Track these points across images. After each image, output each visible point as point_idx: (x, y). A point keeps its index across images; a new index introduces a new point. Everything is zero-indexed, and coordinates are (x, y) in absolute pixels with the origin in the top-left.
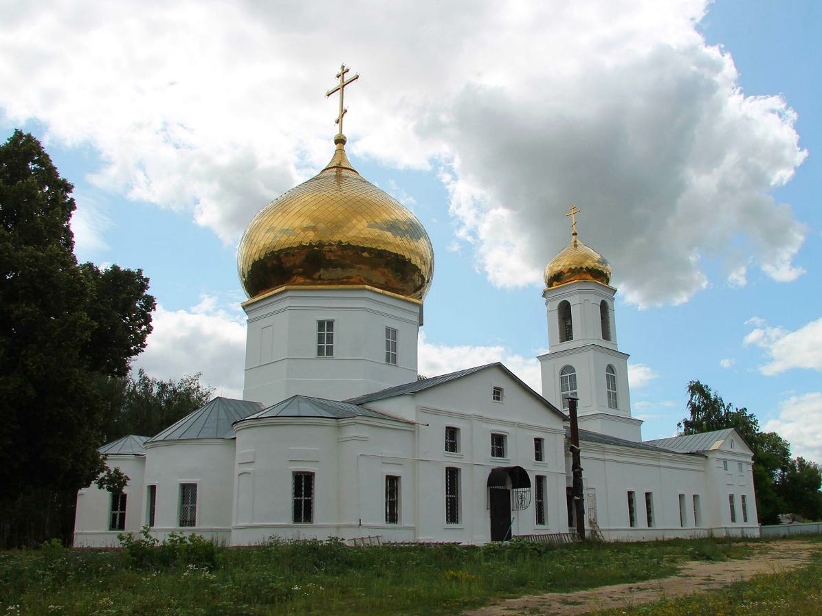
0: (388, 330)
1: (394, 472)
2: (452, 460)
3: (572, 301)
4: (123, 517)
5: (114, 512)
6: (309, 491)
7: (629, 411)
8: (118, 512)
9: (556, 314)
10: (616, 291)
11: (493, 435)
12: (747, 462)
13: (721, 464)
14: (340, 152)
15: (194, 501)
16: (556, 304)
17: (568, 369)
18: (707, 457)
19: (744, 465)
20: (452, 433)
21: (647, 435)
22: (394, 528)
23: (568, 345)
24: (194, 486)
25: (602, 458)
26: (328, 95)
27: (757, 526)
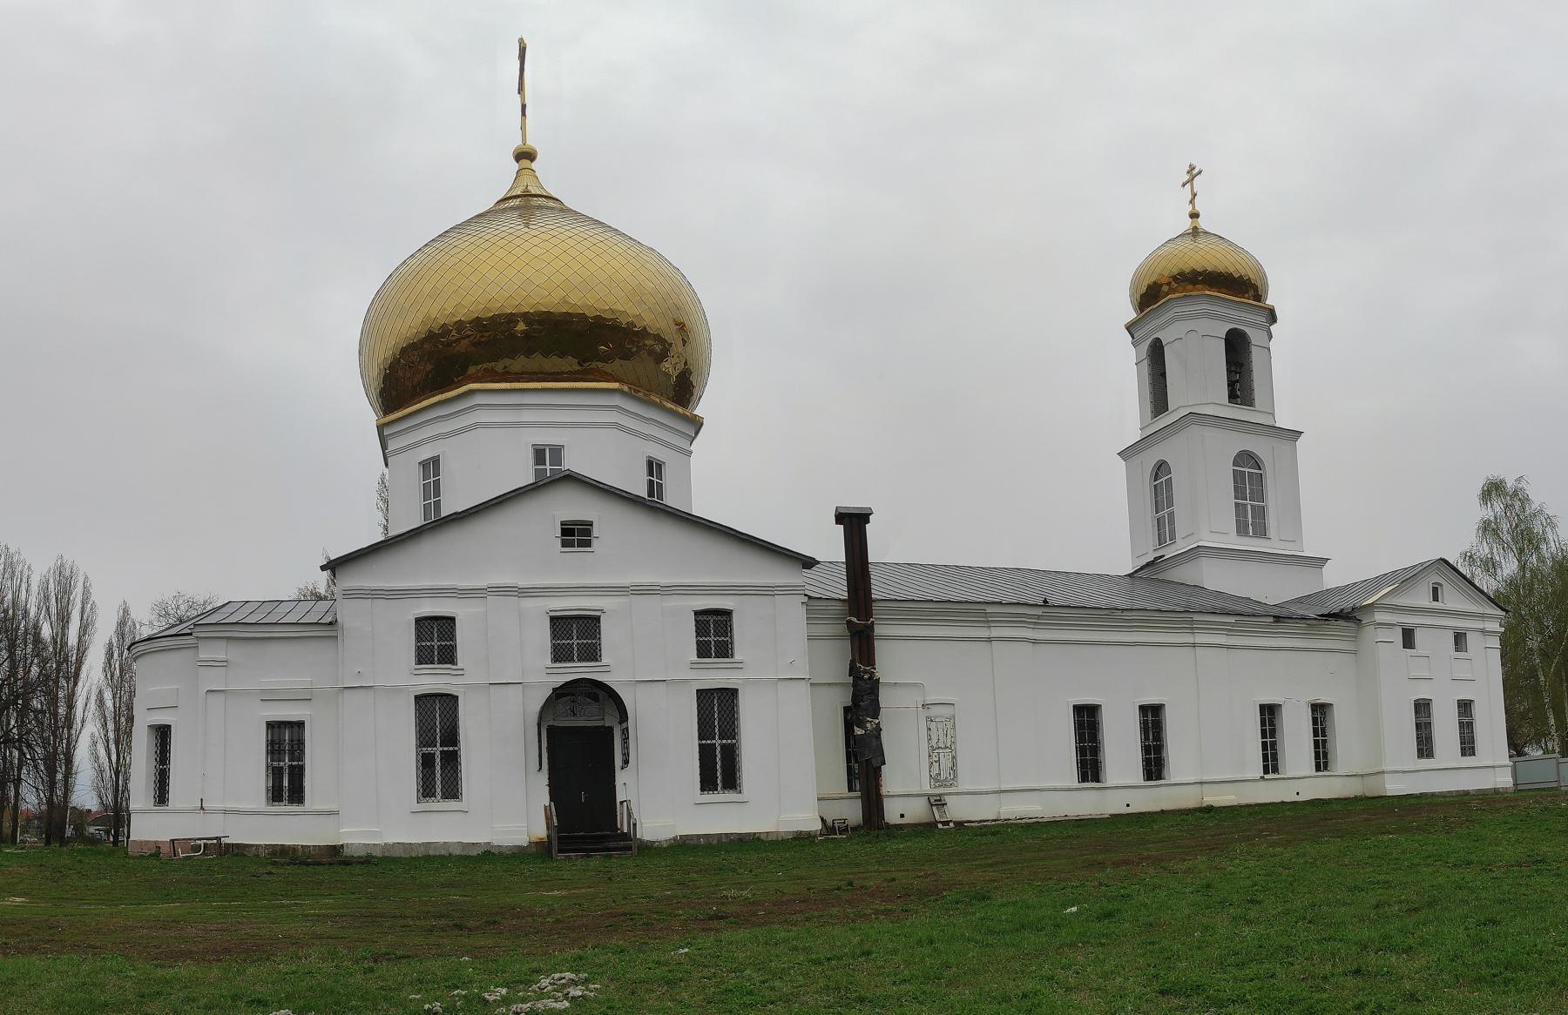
0: (650, 463)
3: (1165, 337)
6: (730, 727)
13: (1397, 636)
21: (146, 632)
22: (296, 814)
27: (1507, 762)
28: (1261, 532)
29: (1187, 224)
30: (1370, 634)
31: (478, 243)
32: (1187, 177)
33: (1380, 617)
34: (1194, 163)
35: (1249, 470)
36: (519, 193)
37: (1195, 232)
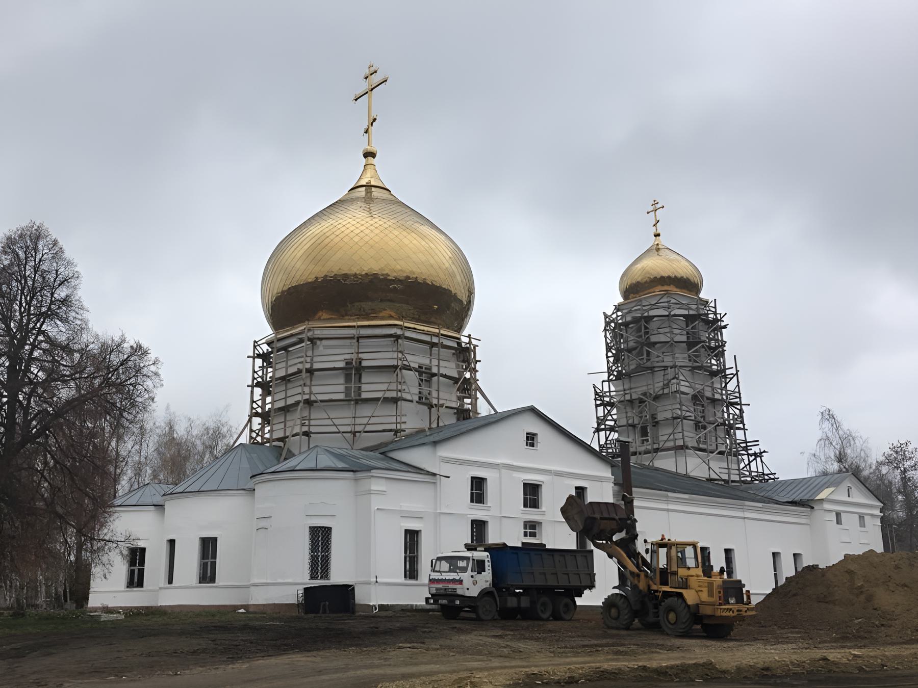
1: (413, 525)
2: (478, 513)
4: (141, 573)
5: (132, 568)
8: (210, 560)
11: (525, 484)
12: (872, 515)
13: (833, 517)
15: (214, 557)
18: (813, 508)
20: (478, 484)
24: (214, 540)
25: (666, 507)
26: (356, 100)
29: (652, 241)
30: (818, 513)
31: (335, 224)
33: (827, 506)
36: (365, 184)
37: (657, 249)
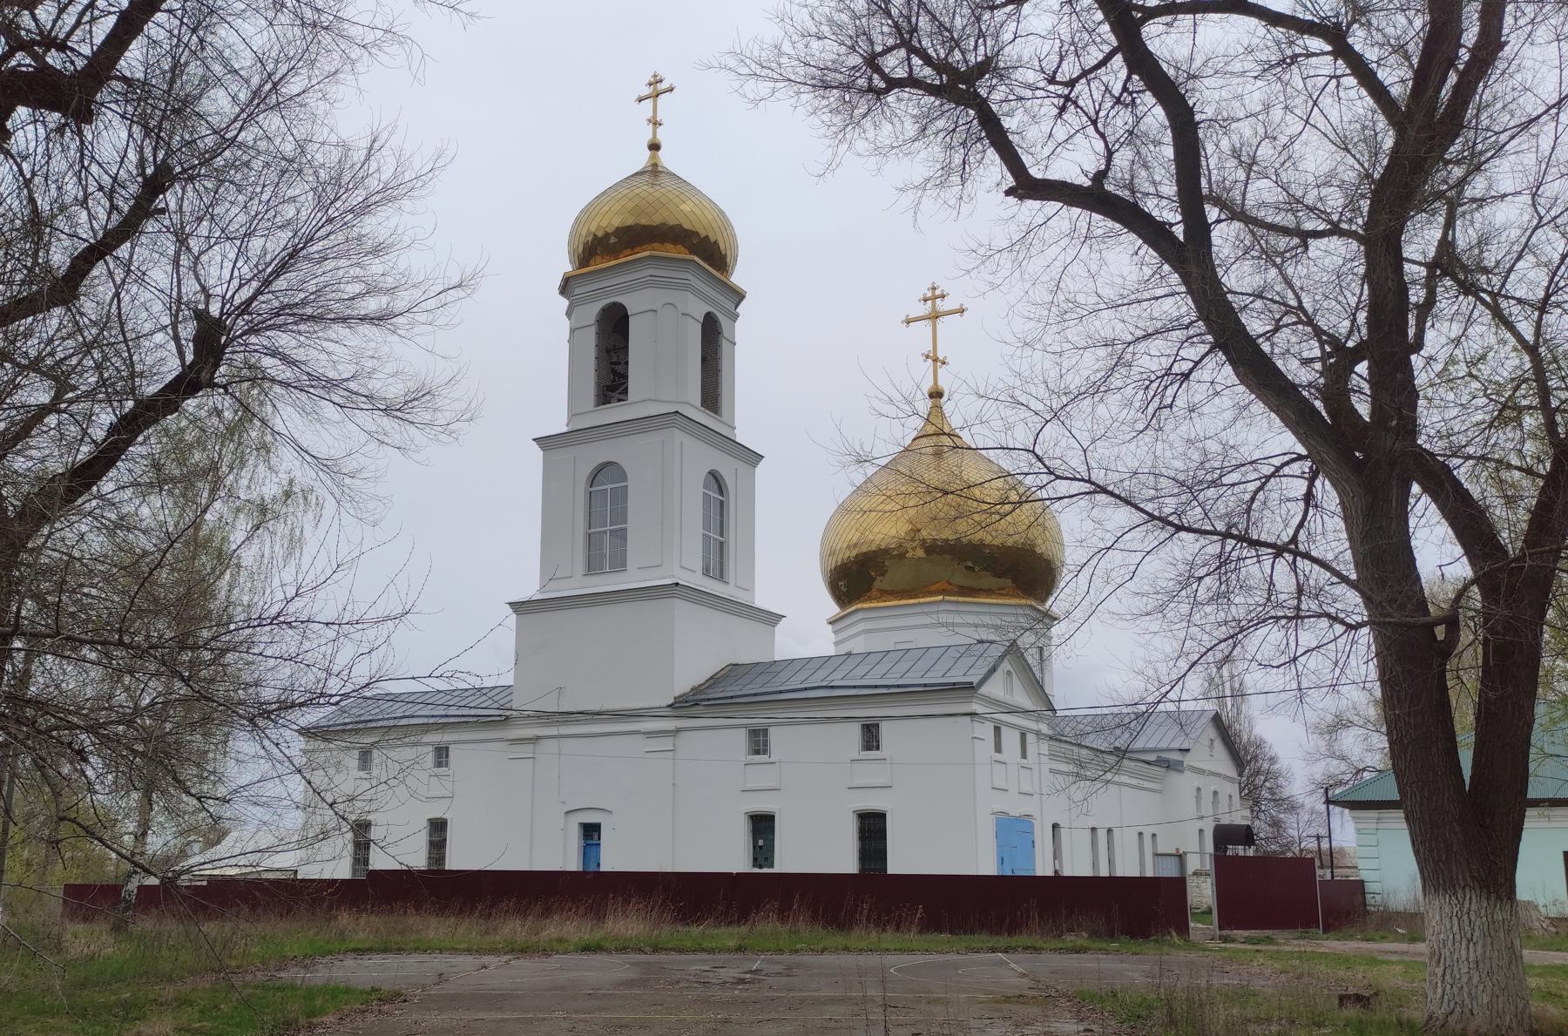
3: (631, 302)
7: (1034, 870)
9: (590, 338)
10: (744, 297)
12: (1038, 733)
14: (937, 408)
16: (592, 311)
17: (605, 471)
19: (1030, 738)
23: (614, 413)
28: (721, 577)
29: (642, 159)
32: (647, 91)
34: (662, 73)
35: (612, 486)
37: (654, 171)
